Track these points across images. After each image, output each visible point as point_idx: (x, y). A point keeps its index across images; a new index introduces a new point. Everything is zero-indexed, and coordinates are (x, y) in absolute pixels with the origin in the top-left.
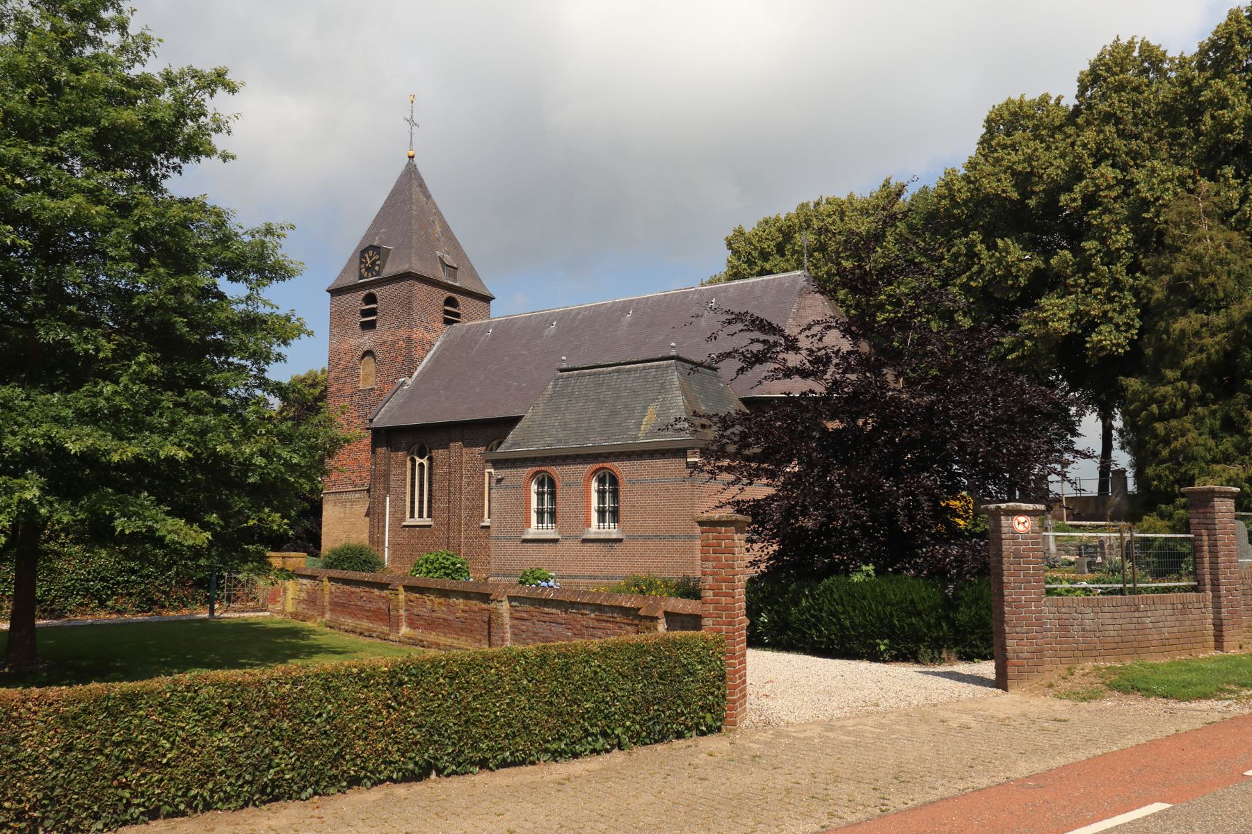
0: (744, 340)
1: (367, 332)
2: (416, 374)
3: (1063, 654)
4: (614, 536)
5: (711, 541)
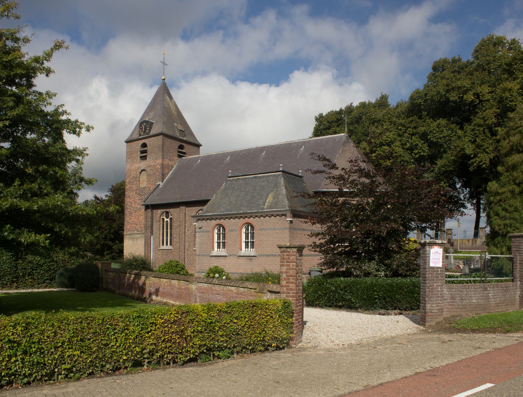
0: (319, 165)
1: (143, 161)
2: (165, 180)
3: (452, 310)
4: (252, 255)
5: (285, 257)
